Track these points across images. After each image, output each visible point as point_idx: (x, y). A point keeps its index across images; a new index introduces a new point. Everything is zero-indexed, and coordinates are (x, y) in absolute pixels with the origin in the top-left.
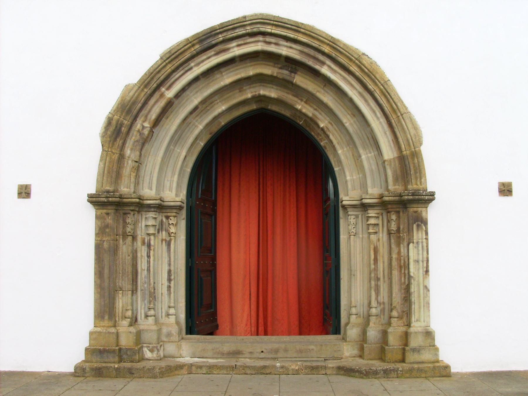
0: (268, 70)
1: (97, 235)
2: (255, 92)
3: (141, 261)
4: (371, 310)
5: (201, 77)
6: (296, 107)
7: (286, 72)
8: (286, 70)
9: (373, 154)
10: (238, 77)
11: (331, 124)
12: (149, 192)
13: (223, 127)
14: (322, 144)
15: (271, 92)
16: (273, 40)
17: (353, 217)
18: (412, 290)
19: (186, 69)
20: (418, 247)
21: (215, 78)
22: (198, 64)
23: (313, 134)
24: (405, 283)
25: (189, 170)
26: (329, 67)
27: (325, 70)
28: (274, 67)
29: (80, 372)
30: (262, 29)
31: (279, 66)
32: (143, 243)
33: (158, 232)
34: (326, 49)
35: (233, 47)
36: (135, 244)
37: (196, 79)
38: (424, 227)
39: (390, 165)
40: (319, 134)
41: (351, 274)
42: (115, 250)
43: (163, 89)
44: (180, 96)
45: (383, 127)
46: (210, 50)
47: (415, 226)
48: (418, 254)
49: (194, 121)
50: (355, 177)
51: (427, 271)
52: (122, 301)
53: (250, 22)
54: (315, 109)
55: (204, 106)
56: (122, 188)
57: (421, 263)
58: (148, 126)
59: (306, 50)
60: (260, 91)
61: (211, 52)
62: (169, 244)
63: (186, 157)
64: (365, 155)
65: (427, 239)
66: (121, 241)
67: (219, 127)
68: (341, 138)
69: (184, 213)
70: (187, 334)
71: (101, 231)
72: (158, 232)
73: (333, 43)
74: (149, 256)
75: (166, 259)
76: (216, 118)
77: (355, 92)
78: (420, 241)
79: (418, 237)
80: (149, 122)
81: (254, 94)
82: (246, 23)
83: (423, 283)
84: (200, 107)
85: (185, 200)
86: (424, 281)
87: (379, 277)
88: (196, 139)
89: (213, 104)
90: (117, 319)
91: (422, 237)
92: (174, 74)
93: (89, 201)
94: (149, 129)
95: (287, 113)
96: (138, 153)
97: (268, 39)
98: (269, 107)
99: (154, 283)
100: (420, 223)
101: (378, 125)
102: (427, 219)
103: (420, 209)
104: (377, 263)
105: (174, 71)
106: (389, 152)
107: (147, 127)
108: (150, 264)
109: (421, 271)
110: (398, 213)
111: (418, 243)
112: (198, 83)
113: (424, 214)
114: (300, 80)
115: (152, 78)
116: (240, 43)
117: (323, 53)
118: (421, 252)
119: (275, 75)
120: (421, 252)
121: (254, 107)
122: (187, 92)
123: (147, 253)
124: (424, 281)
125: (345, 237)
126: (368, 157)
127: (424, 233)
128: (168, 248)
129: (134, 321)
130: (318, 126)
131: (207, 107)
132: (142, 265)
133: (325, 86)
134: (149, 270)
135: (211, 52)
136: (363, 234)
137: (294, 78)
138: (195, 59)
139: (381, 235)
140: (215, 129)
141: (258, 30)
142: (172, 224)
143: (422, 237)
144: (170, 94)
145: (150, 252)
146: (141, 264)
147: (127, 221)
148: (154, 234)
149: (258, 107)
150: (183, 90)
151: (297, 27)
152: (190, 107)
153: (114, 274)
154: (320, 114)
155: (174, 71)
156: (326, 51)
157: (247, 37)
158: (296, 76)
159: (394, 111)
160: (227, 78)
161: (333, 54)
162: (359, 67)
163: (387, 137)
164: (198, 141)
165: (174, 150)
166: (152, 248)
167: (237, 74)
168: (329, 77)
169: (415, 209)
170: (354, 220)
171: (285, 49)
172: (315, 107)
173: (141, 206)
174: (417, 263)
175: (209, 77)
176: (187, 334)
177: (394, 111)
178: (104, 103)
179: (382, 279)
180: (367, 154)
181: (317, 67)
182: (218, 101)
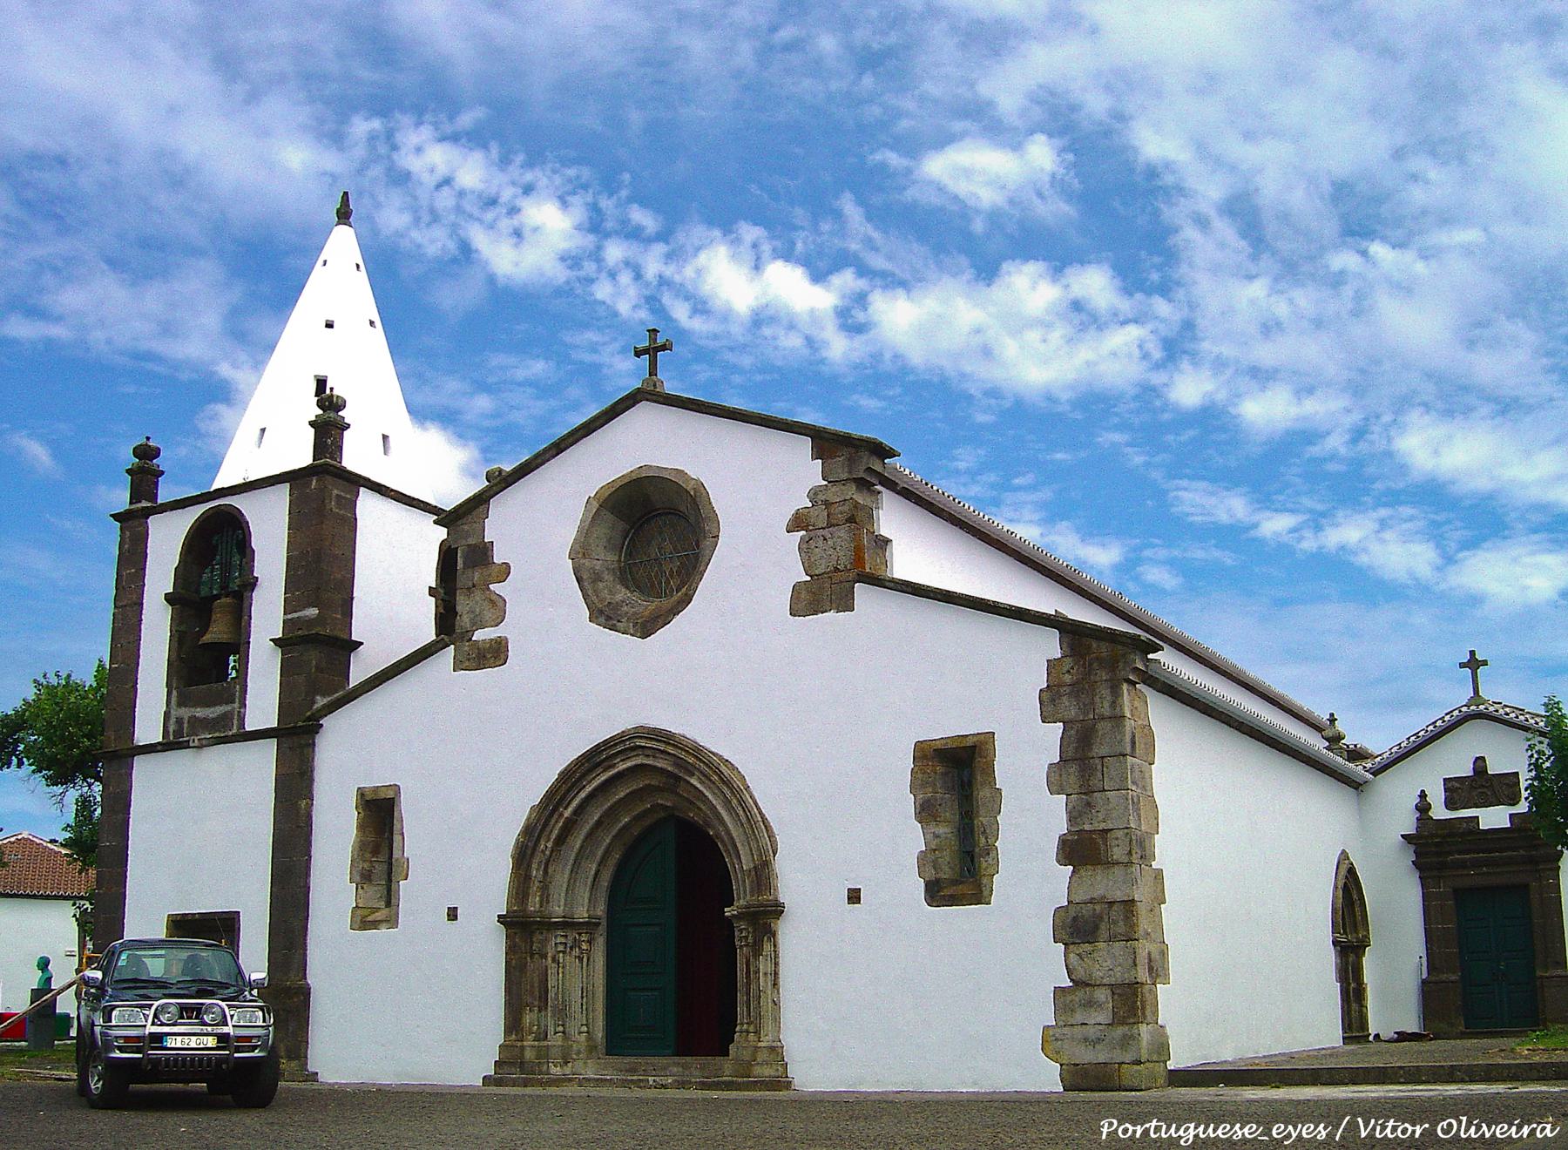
1: (306, 992)
4: (452, 490)
12: (557, 910)
32: (554, 960)
42: (522, 968)
52: (528, 1018)
69: (602, 929)
71: (511, 950)
75: (581, 978)
105: (568, 791)
144: (567, 814)
152: (592, 822)
153: (524, 991)
155: (568, 791)
173: (548, 926)
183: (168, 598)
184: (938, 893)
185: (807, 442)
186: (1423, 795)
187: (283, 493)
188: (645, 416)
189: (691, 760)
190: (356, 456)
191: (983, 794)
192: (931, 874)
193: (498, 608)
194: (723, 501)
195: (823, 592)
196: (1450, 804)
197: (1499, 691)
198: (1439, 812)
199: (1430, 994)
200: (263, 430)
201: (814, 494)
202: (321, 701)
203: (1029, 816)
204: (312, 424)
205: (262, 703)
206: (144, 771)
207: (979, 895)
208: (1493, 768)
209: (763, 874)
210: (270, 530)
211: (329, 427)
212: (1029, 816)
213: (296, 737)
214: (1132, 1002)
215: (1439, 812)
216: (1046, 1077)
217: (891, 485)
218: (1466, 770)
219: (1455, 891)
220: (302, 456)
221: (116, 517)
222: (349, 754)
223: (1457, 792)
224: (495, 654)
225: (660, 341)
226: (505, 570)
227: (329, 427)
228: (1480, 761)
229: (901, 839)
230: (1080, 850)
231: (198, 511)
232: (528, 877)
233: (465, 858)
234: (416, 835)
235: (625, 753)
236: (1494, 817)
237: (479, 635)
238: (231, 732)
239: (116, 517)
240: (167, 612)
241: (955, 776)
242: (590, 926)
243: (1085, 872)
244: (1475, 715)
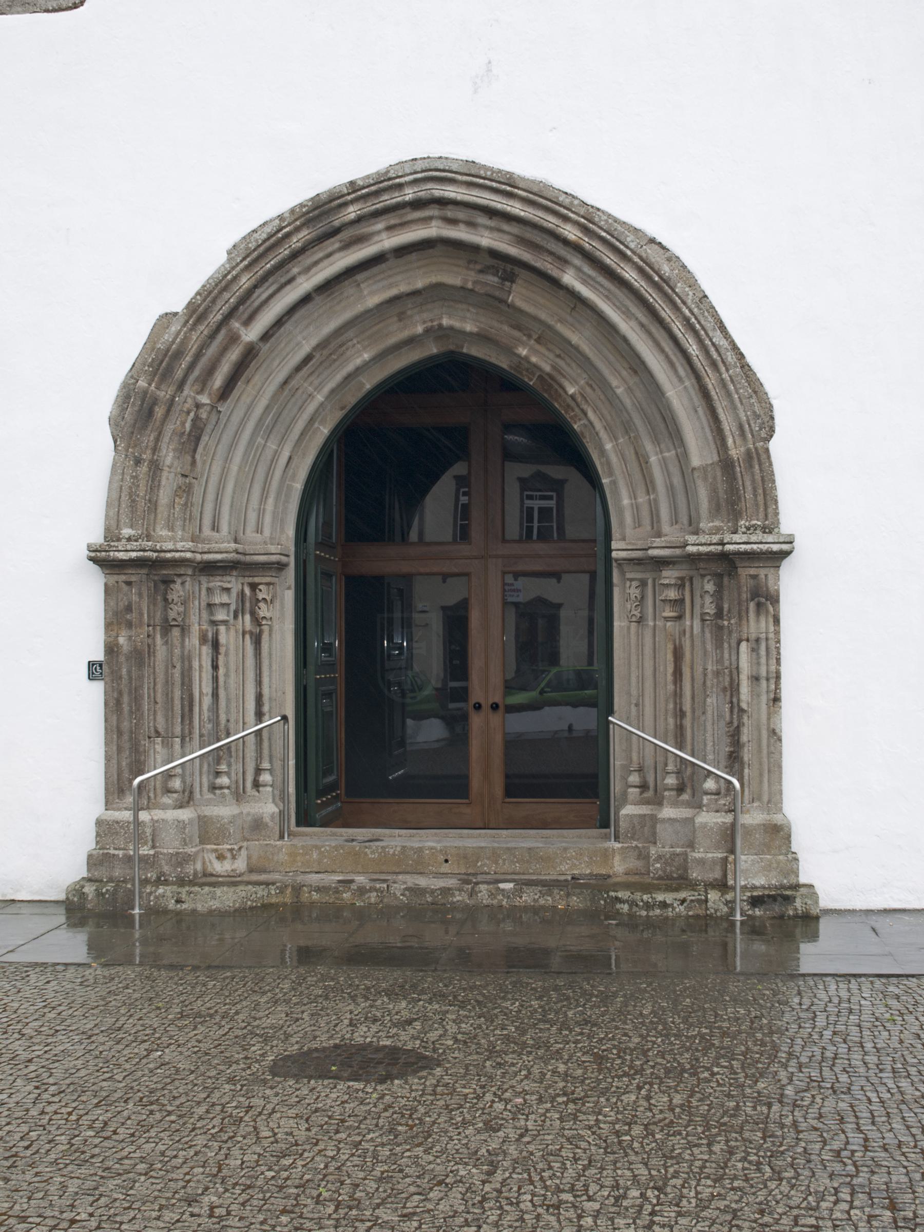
0: (453, 276)
2: (432, 321)
3: (200, 677)
5: (314, 295)
6: (517, 351)
7: (493, 279)
8: (494, 275)
9: (673, 452)
10: (394, 292)
11: (591, 386)
13: (370, 392)
14: (575, 427)
15: (465, 322)
16: (461, 214)
17: (635, 584)
18: (744, 738)
19: (283, 280)
20: (758, 648)
21: (346, 294)
22: (308, 269)
23: (556, 405)
24: (731, 723)
25: (298, 486)
26: (578, 269)
27: (569, 278)
28: (468, 268)
30: (437, 193)
31: (478, 267)
32: (203, 639)
33: (236, 617)
34: (571, 233)
35: (379, 232)
36: (187, 640)
37: (306, 299)
38: (771, 609)
39: (705, 479)
40: (568, 406)
41: (286, 747)
43: (236, 324)
44: (272, 335)
45: (691, 399)
46: (332, 240)
47: (752, 605)
48: (758, 664)
49: (306, 385)
50: (640, 500)
51: (777, 700)
53: (411, 177)
54: (559, 356)
55: (326, 352)
56: (158, 529)
57: (764, 683)
58: (208, 402)
59: (530, 234)
60: (441, 318)
61: (333, 243)
62: (257, 641)
63: (290, 458)
64: (657, 454)
65: (777, 633)
66: (158, 636)
67: (360, 395)
68: (612, 416)
70: (298, 824)
72: (236, 617)
73: (590, 220)
74: (215, 667)
75: (259, 673)
76: (349, 378)
77: (633, 323)
78: (763, 636)
79: (758, 628)
80: (210, 394)
81: (430, 324)
82: (402, 180)
83: (769, 724)
84: (317, 356)
85: (293, 549)
86: (769, 719)
87: (684, 709)
88: (312, 420)
89: (344, 348)
90: (152, 795)
91: (767, 627)
92: (258, 291)
93: (91, 559)
94: (208, 408)
95: (503, 363)
96: (188, 458)
97: (450, 213)
98: (465, 350)
99: (228, 721)
100: (763, 600)
101: (678, 395)
102: (778, 592)
103: (762, 572)
104: (681, 681)
106: (700, 453)
107: (204, 405)
108: (217, 682)
109: (764, 698)
110: (719, 576)
111: (758, 640)
112: (310, 306)
113: (771, 582)
114: (520, 296)
115: (214, 301)
116: (393, 222)
117: (566, 242)
118: (763, 660)
119: (470, 285)
120: (763, 660)
121: (433, 349)
122: (288, 326)
123: (213, 661)
124: (769, 719)
125: (623, 624)
126: (664, 458)
127: (771, 620)
128: (256, 649)
129: (187, 798)
130: (566, 392)
131: (331, 354)
132: (202, 684)
133: (573, 309)
134: (215, 695)
135: (333, 244)
136: (655, 619)
137: (509, 292)
138: (299, 259)
139: (688, 623)
140: (352, 398)
141: (429, 197)
142: (264, 599)
143: (767, 627)
145: (217, 658)
146: (200, 681)
147: (170, 597)
148: (225, 622)
149: (443, 349)
150: (279, 323)
151: (507, 185)
153: (137, 691)
154: (569, 365)
156: (571, 237)
157: (408, 210)
158: (514, 285)
159: (714, 364)
160: (372, 294)
161: (587, 243)
162: (641, 271)
163: (699, 418)
164: (316, 425)
165: (265, 445)
166: (222, 650)
167: (390, 286)
168: (579, 293)
169: (752, 571)
170: (638, 591)
171: (486, 233)
172: (558, 352)
174: (755, 682)
175: (332, 293)
176: (298, 824)
177: (714, 364)
178: (120, 349)
179: (689, 714)
180: (661, 452)
181: (554, 272)
182: (355, 341)
232: (155, 468)
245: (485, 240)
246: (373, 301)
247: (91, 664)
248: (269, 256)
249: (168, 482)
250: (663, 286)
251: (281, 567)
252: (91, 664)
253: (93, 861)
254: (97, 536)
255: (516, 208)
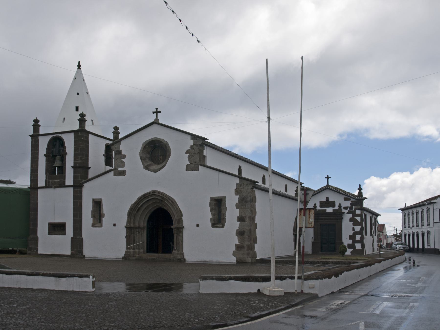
1: (82, 239)
12: (137, 226)
29: (123, 258)
69: (146, 229)
75: (142, 239)
144: (139, 206)
153: (129, 239)
183: (45, 155)
184: (214, 225)
185: (189, 137)
186: (315, 204)
187: (72, 135)
188: (155, 126)
189: (165, 198)
190: (88, 127)
191: (223, 208)
192: (213, 222)
193: (123, 164)
194: (171, 146)
195: (192, 167)
196: (321, 206)
197: (332, 183)
198: (318, 208)
199: (314, 244)
200: (64, 118)
201: (191, 147)
202: (84, 181)
203: (232, 213)
204: (78, 120)
205: (69, 180)
206: (40, 191)
207: (212, 199)
208: (330, 200)
209: (180, 221)
210: (69, 142)
211: (82, 120)
212: (232, 213)
213: (78, 187)
214: (251, 248)
215: (318, 208)
216: (233, 260)
217: (207, 145)
218: (324, 200)
219: (321, 224)
220: (76, 127)
221: (30, 136)
222: (89, 192)
223: (323, 204)
224: (123, 173)
225: (158, 110)
226: (124, 156)
227: (82, 120)
228: (327, 198)
229: (208, 215)
230: (241, 219)
231: (51, 137)
232: (131, 219)
233: (117, 215)
234: (105, 209)
235: (151, 195)
236: (329, 210)
237: (120, 169)
238: (62, 185)
239: (30, 136)
240: (44, 158)
241: (218, 204)
242: (144, 228)
243: (243, 223)
244: (328, 188)
245: (159, 198)
246: (150, 203)
247: (350, 236)
248: (140, 199)
249: (132, 220)
250: (173, 202)
251: (286, 191)
252: (350, 236)
253: (125, 255)
254: (126, 225)
255: (161, 195)
